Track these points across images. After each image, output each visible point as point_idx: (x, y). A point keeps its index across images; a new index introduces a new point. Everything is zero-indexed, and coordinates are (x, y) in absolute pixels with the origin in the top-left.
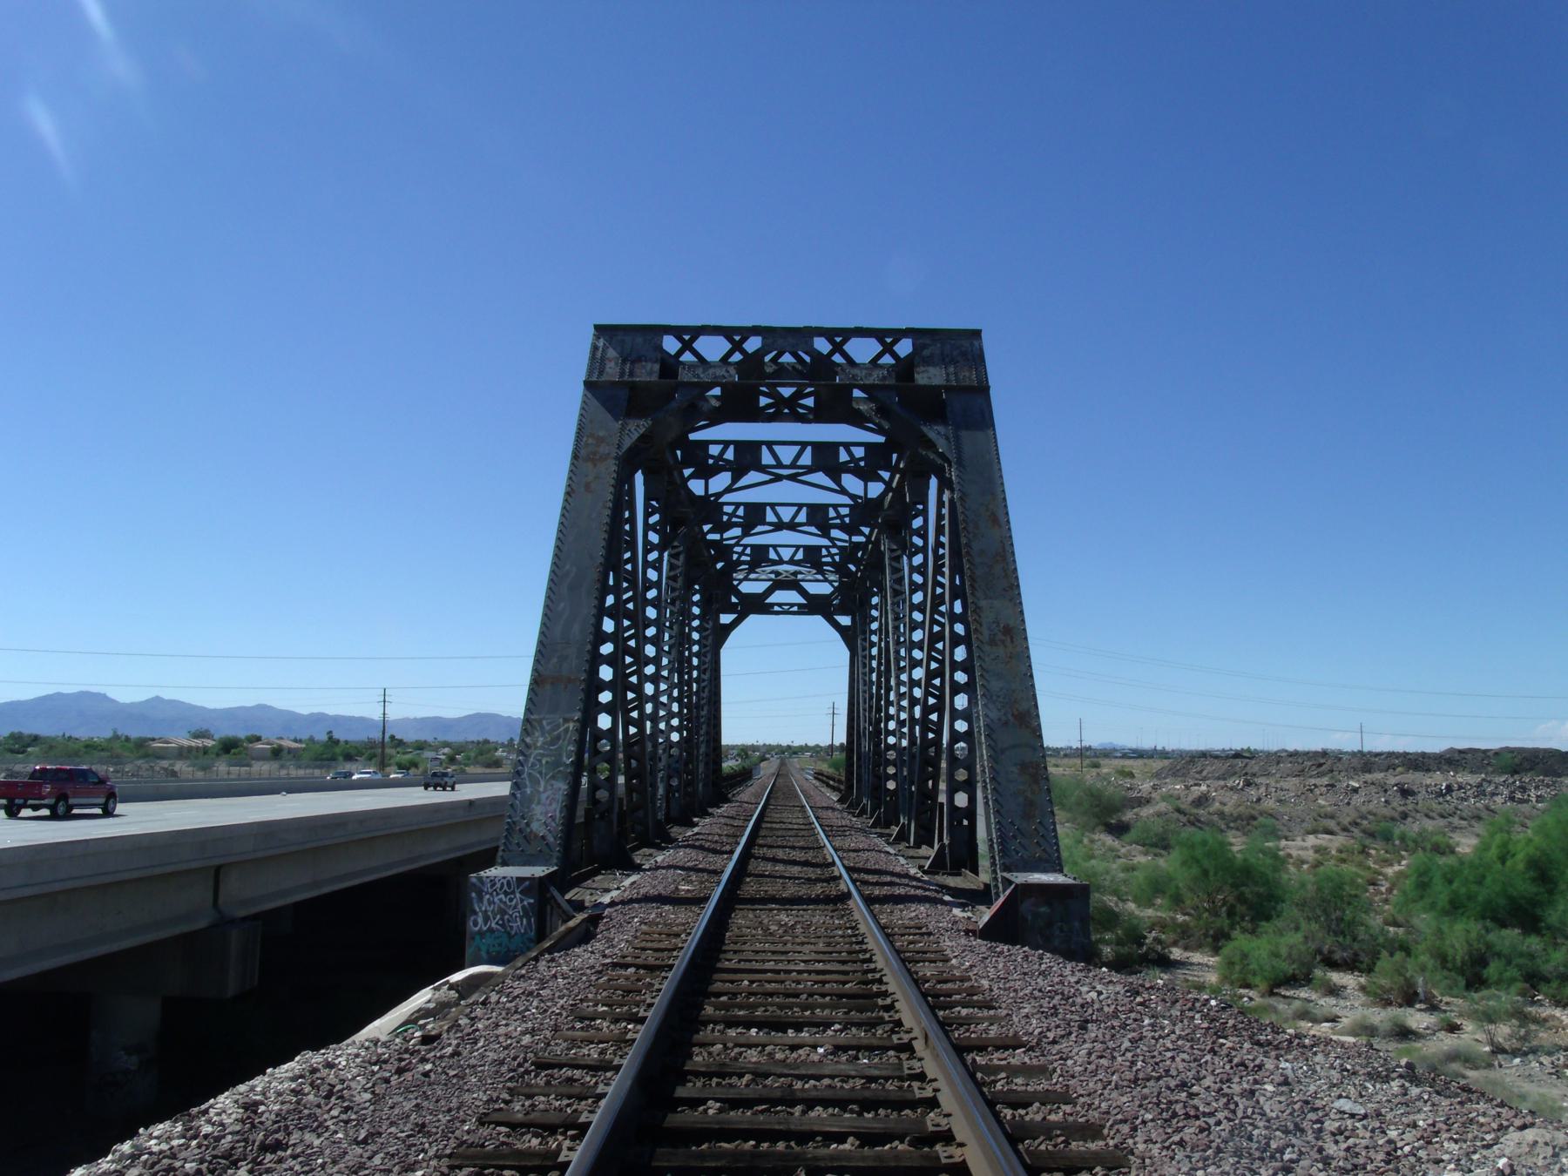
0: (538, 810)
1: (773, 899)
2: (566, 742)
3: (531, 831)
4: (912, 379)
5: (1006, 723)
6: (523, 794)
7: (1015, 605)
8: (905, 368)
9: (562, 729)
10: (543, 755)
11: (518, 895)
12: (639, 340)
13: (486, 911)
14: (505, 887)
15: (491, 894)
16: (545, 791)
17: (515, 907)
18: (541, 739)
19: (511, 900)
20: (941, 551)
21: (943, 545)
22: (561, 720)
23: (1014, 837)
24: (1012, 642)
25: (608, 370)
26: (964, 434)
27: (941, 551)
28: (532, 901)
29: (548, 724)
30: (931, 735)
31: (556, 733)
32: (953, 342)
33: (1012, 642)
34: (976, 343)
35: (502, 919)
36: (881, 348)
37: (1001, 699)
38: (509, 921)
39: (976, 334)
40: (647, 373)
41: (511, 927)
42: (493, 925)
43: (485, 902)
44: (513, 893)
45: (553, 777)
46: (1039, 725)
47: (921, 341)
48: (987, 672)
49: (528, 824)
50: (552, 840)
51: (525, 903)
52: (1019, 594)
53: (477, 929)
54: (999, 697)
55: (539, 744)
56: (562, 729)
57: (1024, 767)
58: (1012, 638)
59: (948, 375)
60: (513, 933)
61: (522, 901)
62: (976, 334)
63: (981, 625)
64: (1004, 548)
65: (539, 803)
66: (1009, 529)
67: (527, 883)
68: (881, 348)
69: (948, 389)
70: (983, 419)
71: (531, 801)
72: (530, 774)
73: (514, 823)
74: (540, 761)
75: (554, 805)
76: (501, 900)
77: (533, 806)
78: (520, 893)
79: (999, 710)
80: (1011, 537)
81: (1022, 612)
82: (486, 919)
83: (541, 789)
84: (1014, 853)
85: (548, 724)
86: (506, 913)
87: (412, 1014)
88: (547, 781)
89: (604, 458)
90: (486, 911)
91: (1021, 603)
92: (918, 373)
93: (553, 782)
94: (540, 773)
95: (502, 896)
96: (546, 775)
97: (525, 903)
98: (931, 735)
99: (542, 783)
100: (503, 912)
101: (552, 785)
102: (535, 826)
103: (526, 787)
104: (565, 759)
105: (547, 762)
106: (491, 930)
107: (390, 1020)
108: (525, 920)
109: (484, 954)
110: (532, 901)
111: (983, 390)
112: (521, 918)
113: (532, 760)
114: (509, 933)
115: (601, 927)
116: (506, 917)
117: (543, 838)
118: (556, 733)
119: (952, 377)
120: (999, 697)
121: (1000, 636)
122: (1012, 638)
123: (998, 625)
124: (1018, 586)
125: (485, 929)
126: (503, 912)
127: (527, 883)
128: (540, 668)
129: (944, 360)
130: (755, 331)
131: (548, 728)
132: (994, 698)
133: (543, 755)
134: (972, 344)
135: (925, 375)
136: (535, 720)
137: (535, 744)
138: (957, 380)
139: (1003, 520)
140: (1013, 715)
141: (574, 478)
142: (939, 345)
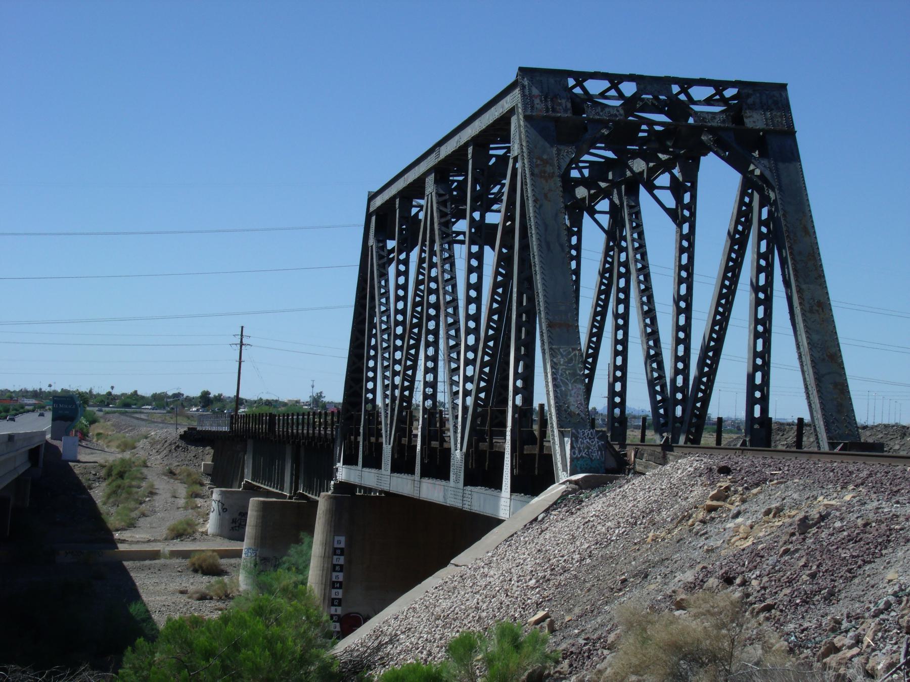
0: (571, 400)
1: (144, 542)
2: (577, 362)
3: (571, 411)
4: (743, 123)
5: (823, 360)
6: (561, 390)
7: (823, 288)
8: (630, 104)
9: (572, 354)
10: (566, 369)
11: (596, 440)
12: (552, 81)
13: (580, 447)
14: (590, 435)
15: (582, 439)
16: (572, 390)
17: (594, 446)
18: (562, 360)
19: (592, 442)
20: (423, 255)
21: (425, 251)
22: (571, 350)
23: (833, 422)
24: (823, 311)
25: (536, 106)
26: (781, 165)
27: (423, 255)
28: (603, 443)
29: (564, 351)
30: (405, 404)
31: (570, 356)
32: (767, 92)
33: (823, 311)
34: (784, 94)
35: (588, 451)
36: (680, 90)
37: (819, 346)
38: (591, 453)
39: (783, 87)
40: (564, 112)
41: (593, 456)
42: (584, 455)
43: (579, 442)
44: (594, 438)
45: (575, 382)
46: (842, 362)
47: (746, 91)
48: (810, 329)
49: (568, 407)
50: (583, 416)
51: (600, 443)
52: (825, 281)
53: (575, 456)
54: (818, 344)
55: (562, 363)
56: (572, 354)
57: (836, 385)
58: (823, 309)
59: (766, 119)
60: (593, 458)
61: (598, 442)
62: (783, 87)
63: (804, 300)
64: (813, 249)
65: (571, 396)
66: (816, 238)
67: (601, 433)
68: (680, 90)
69: (766, 132)
70: (792, 155)
71: (566, 395)
72: (561, 380)
73: (561, 406)
74: (565, 372)
75: (580, 397)
76: (587, 442)
77: (569, 397)
78: (598, 438)
79: (819, 352)
80: (817, 243)
81: (827, 293)
82: (580, 451)
83: (570, 388)
84: (833, 431)
85: (564, 351)
86: (590, 448)
87: (563, 493)
88: (572, 384)
89: (551, 176)
90: (580, 447)
91: (826, 287)
92: (747, 117)
93: (576, 384)
94: (567, 379)
95: (588, 440)
96: (571, 380)
97: (600, 443)
98: (405, 404)
99: (570, 385)
100: (589, 448)
101: (576, 386)
102: (572, 408)
103: (561, 386)
104: (579, 372)
105: (569, 373)
106: (582, 457)
107: (543, 500)
108: (599, 452)
109: (579, 469)
110: (603, 443)
111: (790, 133)
112: (598, 451)
113: (560, 372)
114: (591, 459)
115: (164, 536)
116: (590, 450)
117: (578, 414)
118: (570, 356)
119: (770, 123)
120: (818, 344)
121: (815, 308)
122: (823, 309)
123: (814, 301)
124: (824, 276)
125: (579, 456)
126: (589, 448)
127: (601, 433)
128: (550, 318)
129: (765, 107)
130: (631, 78)
131: (564, 353)
132: (816, 345)
133: (566, 369)
134: (781, 95)
135: (751, 119)
136: (556, 349)
137: (560, 363)
138: (773, 125)
139: (811, 231)
140: (827, 356)
141: (535, 190)
142: (758, 95)
